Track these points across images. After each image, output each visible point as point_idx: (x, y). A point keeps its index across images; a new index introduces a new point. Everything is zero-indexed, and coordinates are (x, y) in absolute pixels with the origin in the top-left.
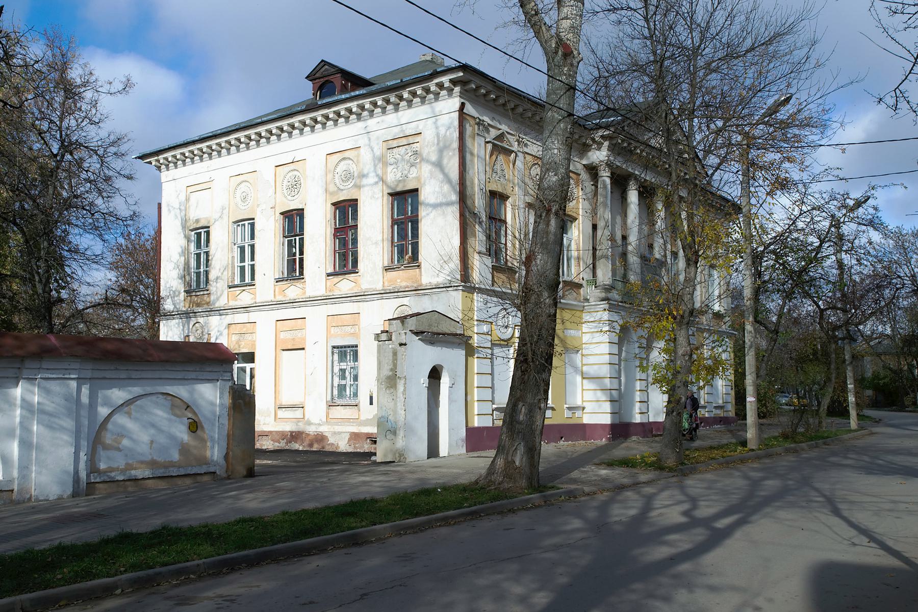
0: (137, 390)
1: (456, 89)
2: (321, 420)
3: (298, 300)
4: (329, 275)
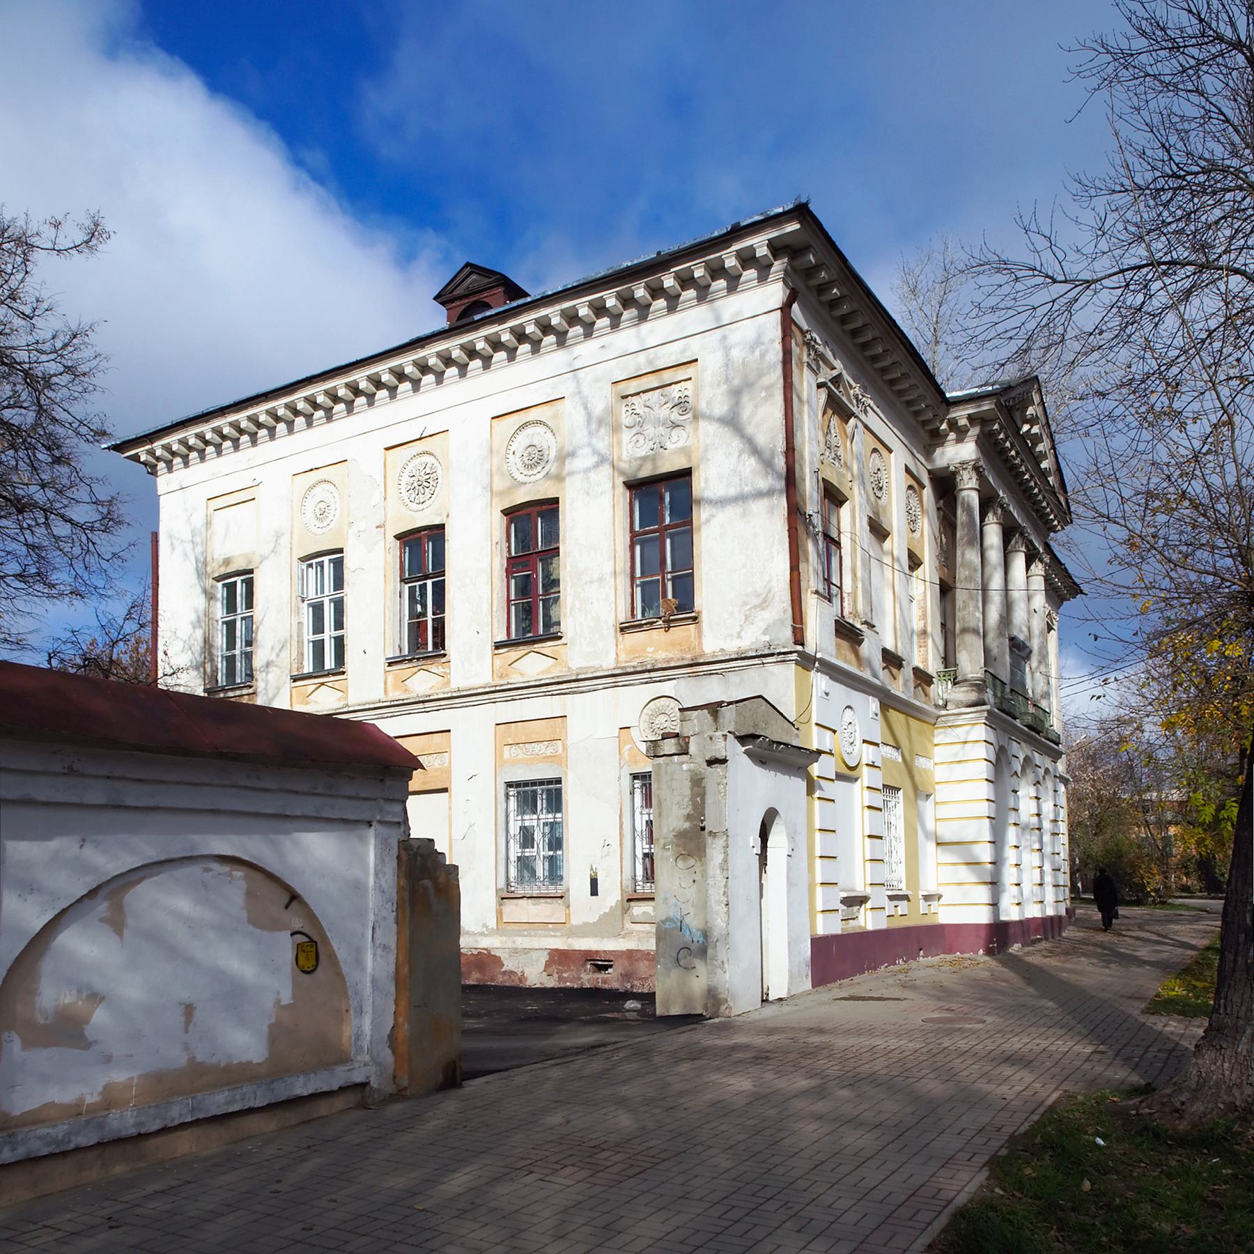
0: (145, 848)
1: (776, 263)
2: (484, 925)
3: (436, 697)
4: (498, 646)
